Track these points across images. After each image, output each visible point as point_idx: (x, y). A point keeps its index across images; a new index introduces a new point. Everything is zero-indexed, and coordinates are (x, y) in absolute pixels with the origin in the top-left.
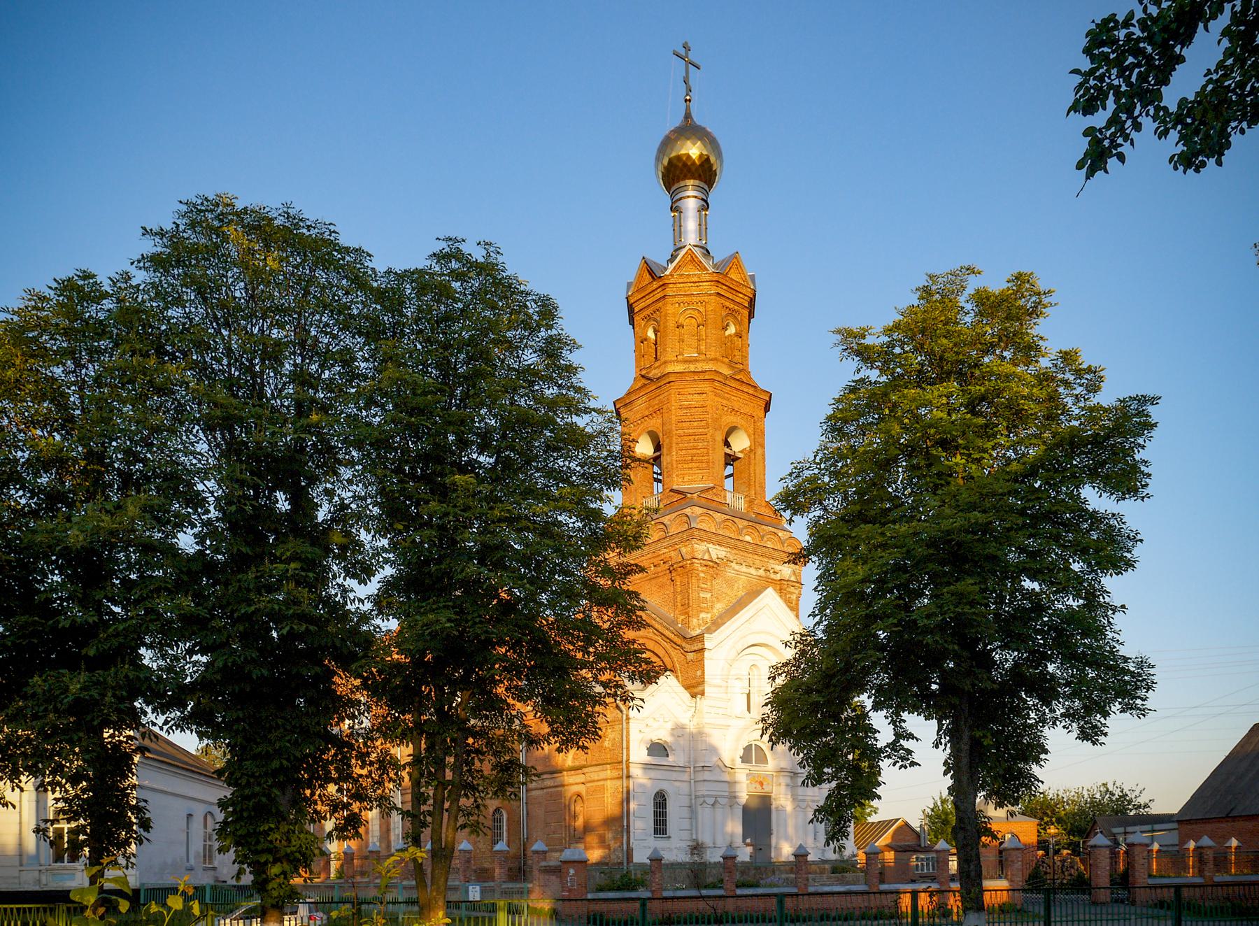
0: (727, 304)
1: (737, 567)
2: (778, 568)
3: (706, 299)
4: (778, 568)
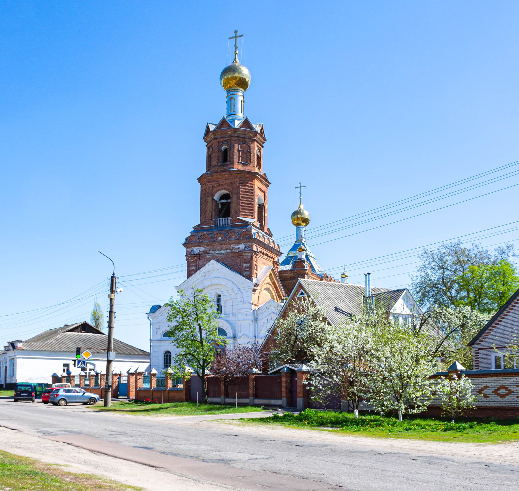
0: (222, 140)
1: (213, 252)
2: (237, 247)
4: (237, 247)
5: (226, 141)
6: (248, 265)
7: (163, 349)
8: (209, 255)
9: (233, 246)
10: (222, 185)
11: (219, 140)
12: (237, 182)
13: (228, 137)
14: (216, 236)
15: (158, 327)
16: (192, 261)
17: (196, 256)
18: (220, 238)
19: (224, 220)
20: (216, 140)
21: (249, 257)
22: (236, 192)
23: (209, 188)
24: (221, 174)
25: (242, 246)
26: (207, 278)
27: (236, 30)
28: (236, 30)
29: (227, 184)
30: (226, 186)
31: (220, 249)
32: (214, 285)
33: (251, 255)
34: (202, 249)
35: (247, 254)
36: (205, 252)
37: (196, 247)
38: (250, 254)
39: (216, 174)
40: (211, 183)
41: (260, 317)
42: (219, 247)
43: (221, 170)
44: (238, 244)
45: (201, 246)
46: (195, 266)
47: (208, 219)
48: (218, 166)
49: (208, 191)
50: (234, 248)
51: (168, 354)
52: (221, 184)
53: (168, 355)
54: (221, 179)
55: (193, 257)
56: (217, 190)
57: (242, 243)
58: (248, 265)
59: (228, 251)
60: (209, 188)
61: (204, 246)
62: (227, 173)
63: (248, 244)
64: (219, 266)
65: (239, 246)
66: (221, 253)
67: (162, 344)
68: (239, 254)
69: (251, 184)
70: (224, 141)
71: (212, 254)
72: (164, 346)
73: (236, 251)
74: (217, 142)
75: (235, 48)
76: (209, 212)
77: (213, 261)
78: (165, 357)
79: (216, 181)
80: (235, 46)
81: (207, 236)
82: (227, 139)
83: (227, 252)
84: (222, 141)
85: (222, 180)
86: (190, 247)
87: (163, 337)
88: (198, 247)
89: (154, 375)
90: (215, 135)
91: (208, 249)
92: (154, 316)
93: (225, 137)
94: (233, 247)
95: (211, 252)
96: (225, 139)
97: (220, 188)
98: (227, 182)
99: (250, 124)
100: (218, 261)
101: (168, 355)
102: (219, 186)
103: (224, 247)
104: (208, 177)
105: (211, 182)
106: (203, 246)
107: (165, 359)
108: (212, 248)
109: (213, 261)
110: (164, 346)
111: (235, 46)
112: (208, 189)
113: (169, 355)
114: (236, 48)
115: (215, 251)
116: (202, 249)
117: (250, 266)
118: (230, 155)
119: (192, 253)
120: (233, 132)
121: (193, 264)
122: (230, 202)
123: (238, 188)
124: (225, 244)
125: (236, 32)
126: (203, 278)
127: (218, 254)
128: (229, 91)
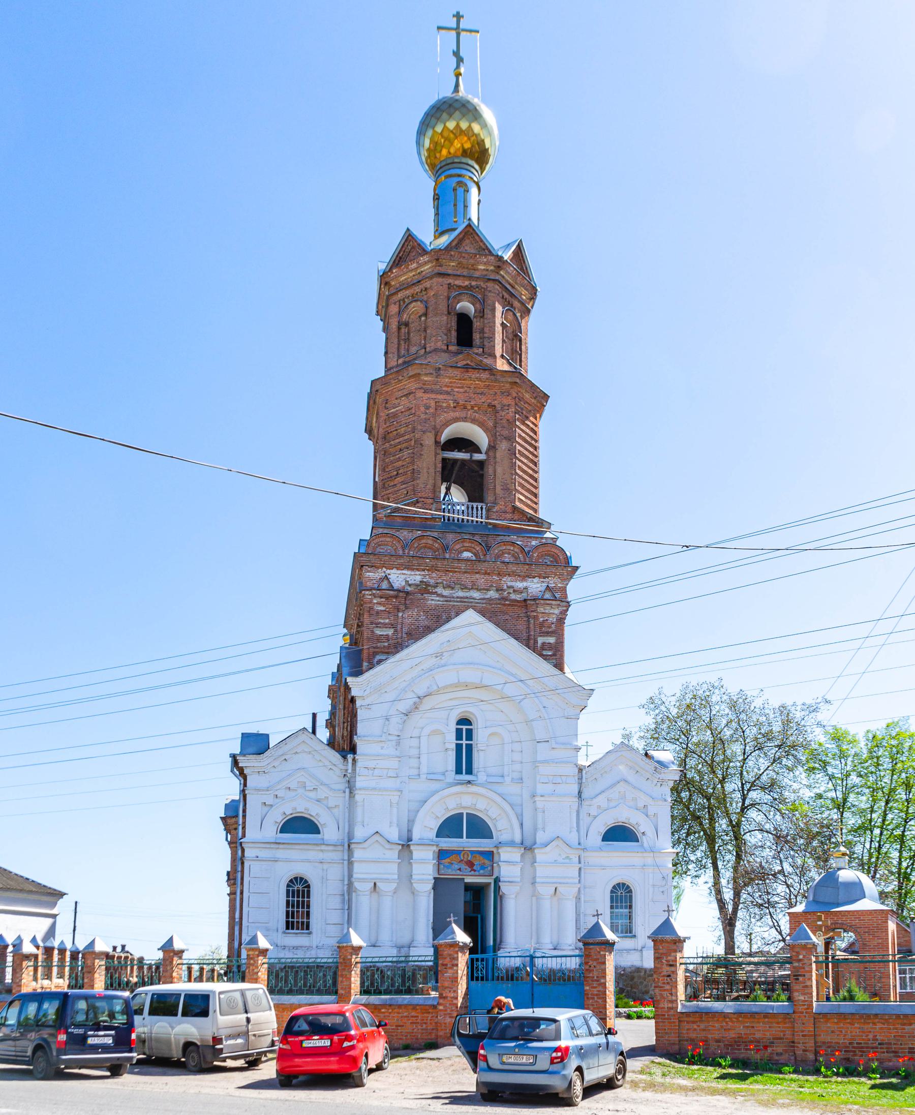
0: (458, 282)
1: (446, 592)
2: (520, 585)
3: (427, 284)
4: (520, 585)
5: (469, 288)
6: (552, 640)
7: (286, 872)
8: (434, 597)
9: (507, 581)
10: (465, 408)
11: (451, 281)
12: (509, 405)
13: (477, 278)
14: (457, 547)
15: (270, 800)
16: (382, 608)
17: (396, 597)
18: (466, 555)
19: (477, 508)
20: (440, 280)
21: (553, 619)
22: (505, 433)
23: (427, 408)
24: (466, 375)
25: (535, 586)
26: (443, 662)
27: (458, 13)
28: (458, 13)
29: (479, 408)
30: (475, 412)
31: (469, 585)
32: (467, 686)
33: (561, 613)
34: (416, 577)
35: (548, 610)
36: (424, 589)
37: (398, 569)
38: (557, 611)
39: (450, 370)
40: (433, 396)
41: (885, 726)
42: (466, 579)
43: (465, 363)
44: (524, 578)
45: (413, 570)
46: (392, 626)
47: (423, 495)
48: (447, 351)
49: (423, 416)
50: (512, 587)
51: (298, 887)
52: (461, 402)
53: (298, 891)
54: (462, 390)
55: (388, 598)
56: (450, 418)
57: (534, 577)
58: (552, 640)
59: (492, 594)
60: (427, 408)
61: (424, 570)
62: (485, 375)
63: (552, 582)
64: (488, 630)
65: (525, 584)
66: (471, 598)
67: (281, 853)
68: (527, 604)
69: (533, 423)
70: (466, 288)
71: (439, 595)
72: (287, 861)
73: (513, 596)
74: (446, 286)
75: (455, 59)
76: (426, 475)
77: (470, 616)
78: (288, 896)
79: (448, 393)
80: (456, 54)
81: (430, 542)
82: (474, 283)
83: (487, 597)
84: (459, 287)
85: (465, 392)
86: (378, 568)
87: (281, 832)
88: (404, 572)
89: (264, 952)
90: (441, 266)
91: (432, 582)
92: (256, 764)
93: (470, 278)
94: (510, 584)
95: (439, 590)
96: (467, 283)
97: (457, 414)
98: (479, 402)
99: (524, 262)
100: (482, 613)
101: (298, 891)
102: (455, 407)
103: (481, 580)
104: (426, 375)
105: (432, 391)
106: (418, 570)
107: (308, 897)
108: (447, 578)
109: (470, 616)
110: (287, 861)
111: (456, 54)
112: (422, 409)
113: (303, 891)
114: (460, 60)
115: (453, 588)
116: (416, 577)
117: (556, 643)
118: (482, 331)
119: (385, 585)
120: (492, 268)
121: (384, 618)
122: (481, 463)
123: (511, 423)
124: (486, 573)
125: (458, 16)
126: (433, 661)
127: (461, 598)
128: (450, 166)
